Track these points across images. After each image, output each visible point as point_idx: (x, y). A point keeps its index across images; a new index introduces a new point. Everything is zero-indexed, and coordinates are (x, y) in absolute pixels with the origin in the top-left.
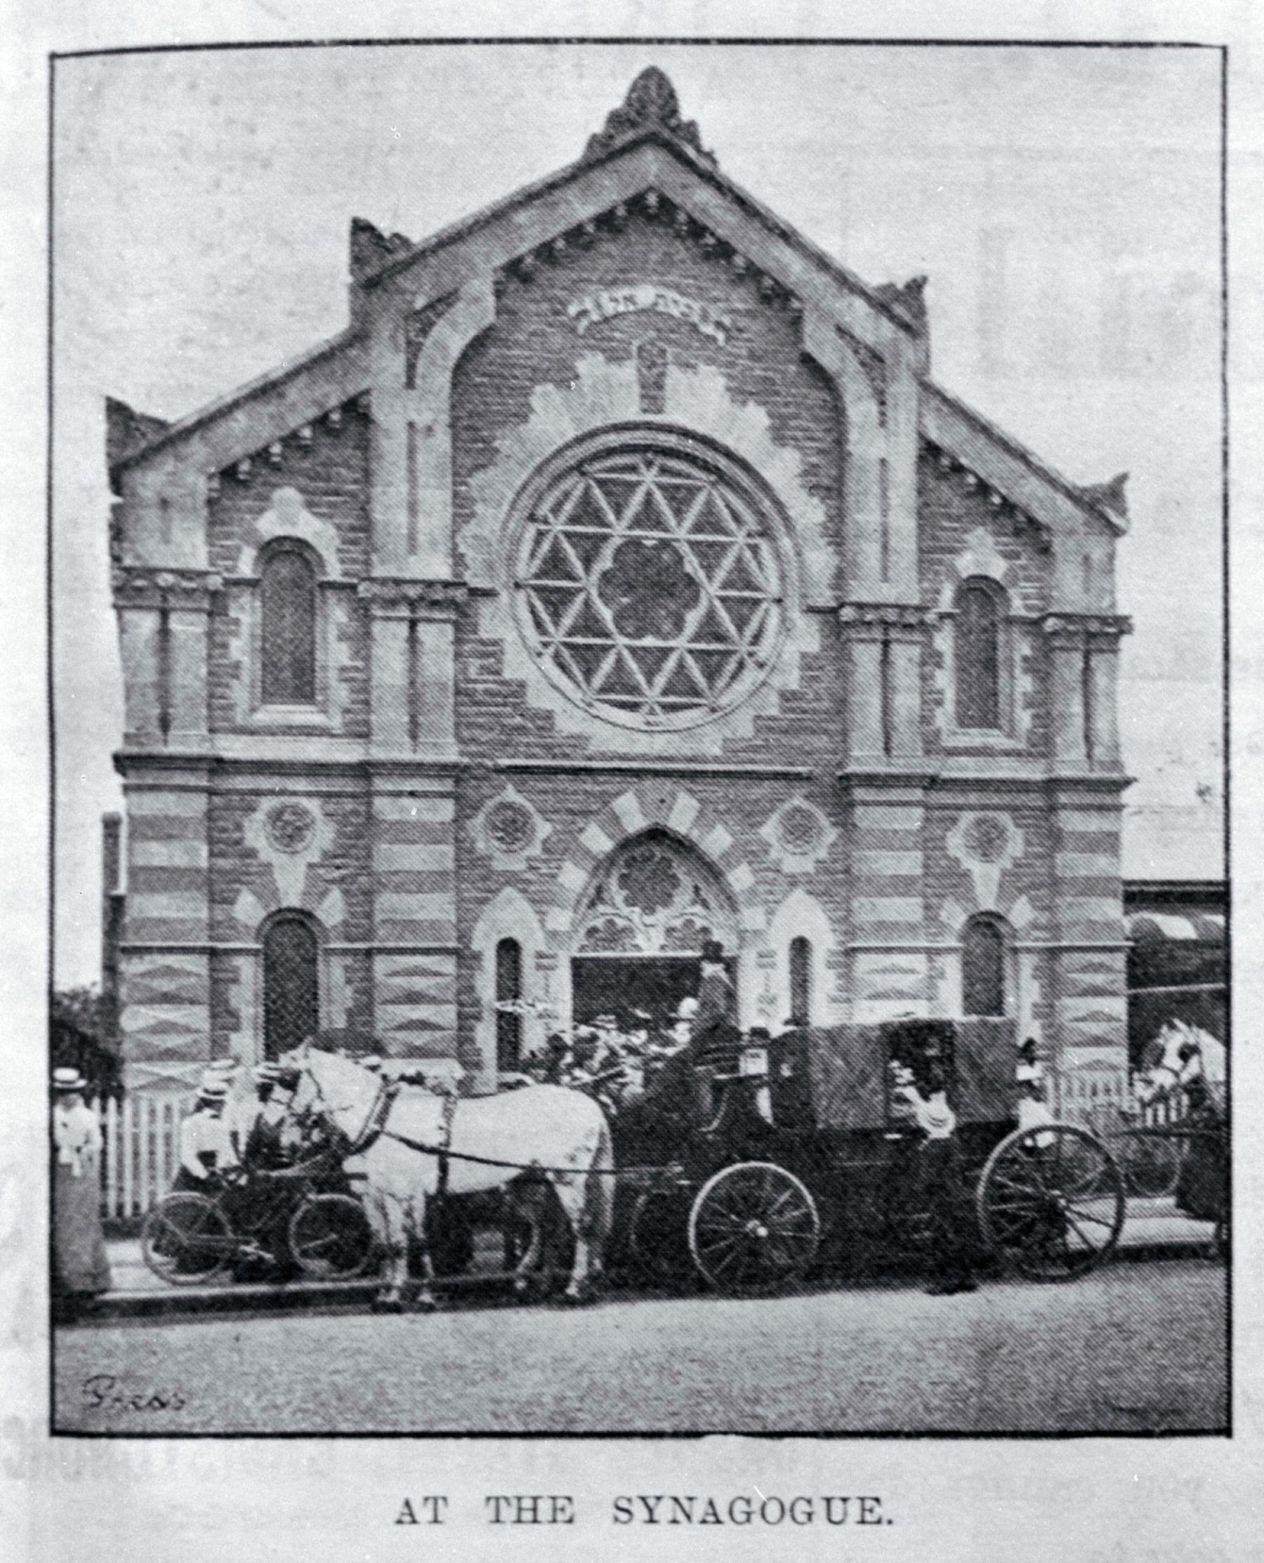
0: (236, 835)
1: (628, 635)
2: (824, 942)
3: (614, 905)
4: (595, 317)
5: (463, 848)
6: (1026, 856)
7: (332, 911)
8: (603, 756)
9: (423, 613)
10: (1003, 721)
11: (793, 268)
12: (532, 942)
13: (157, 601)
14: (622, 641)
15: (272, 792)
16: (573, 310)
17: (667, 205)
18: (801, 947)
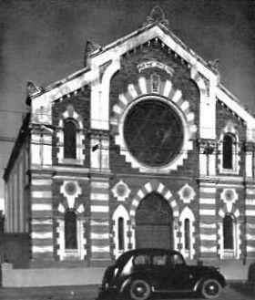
2: (192, 219)
5: (111, 195)
12: (126, 218)
17: (160, 41)
18: (187, 220)
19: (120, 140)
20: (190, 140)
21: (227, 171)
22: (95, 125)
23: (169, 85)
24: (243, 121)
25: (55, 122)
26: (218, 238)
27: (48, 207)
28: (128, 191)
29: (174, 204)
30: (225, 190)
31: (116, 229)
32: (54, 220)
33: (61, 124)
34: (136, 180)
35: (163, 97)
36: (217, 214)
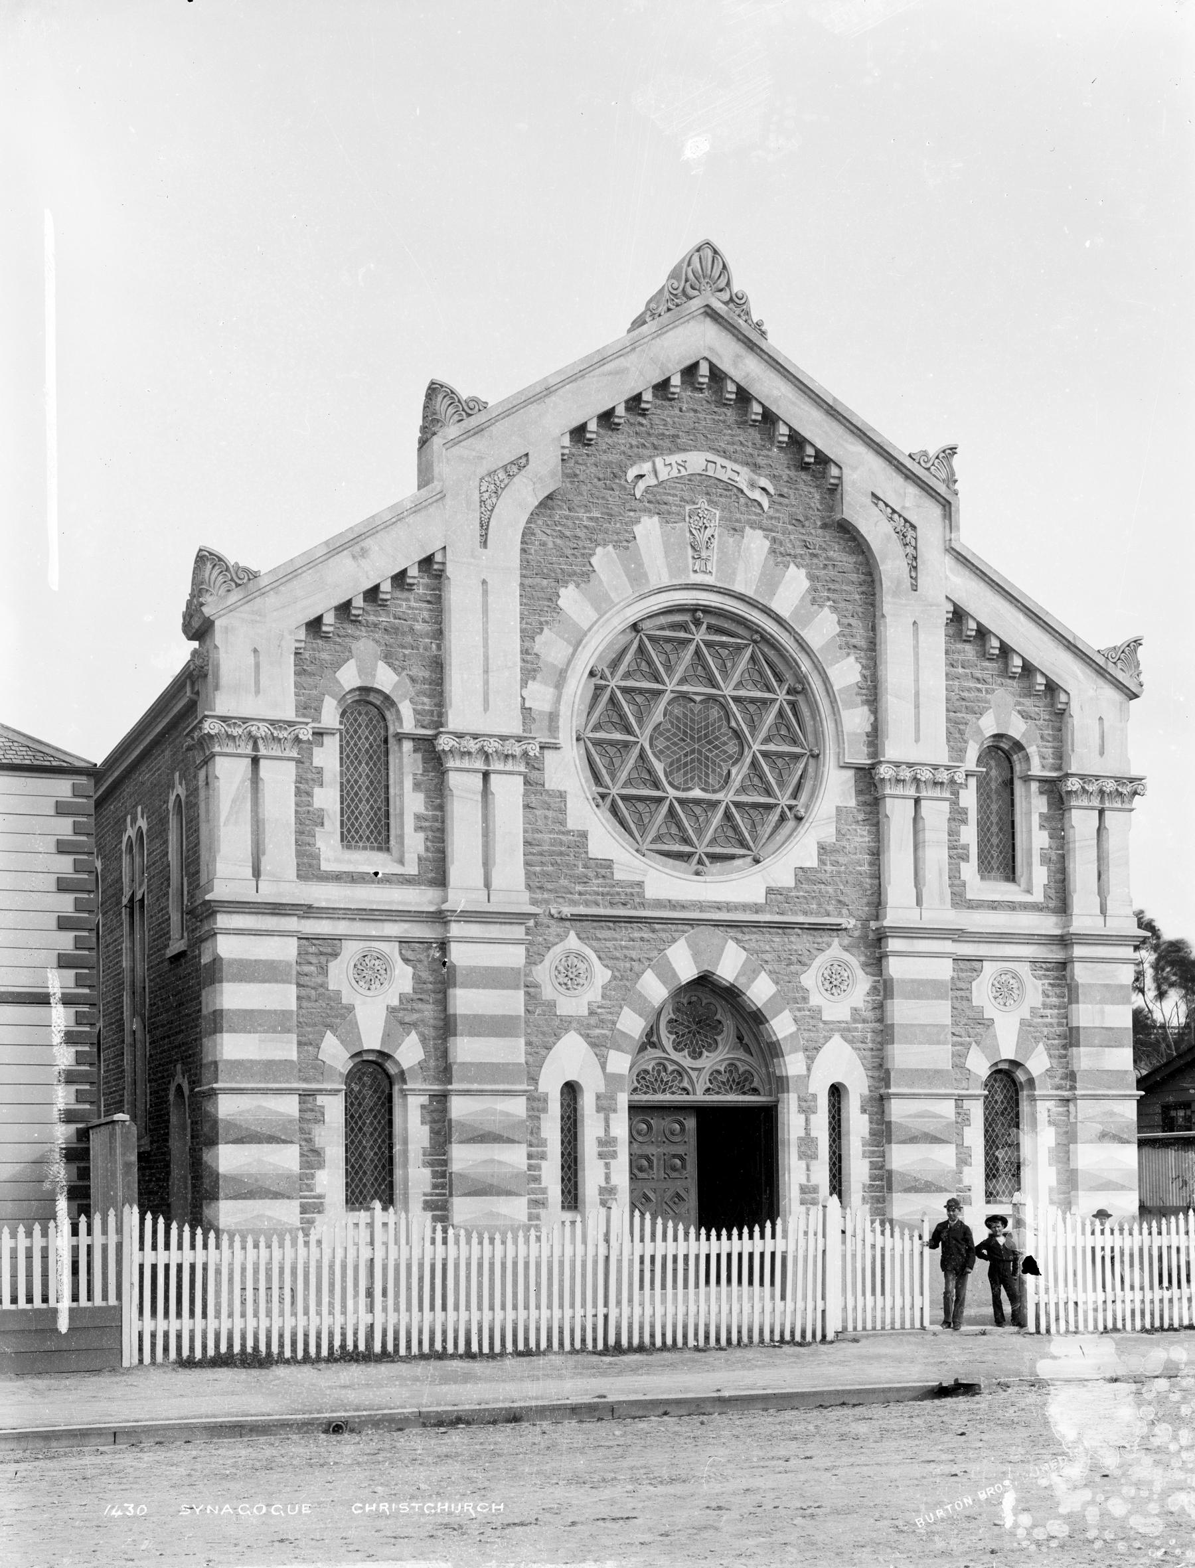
0: (319, 980)
2: (858, 1087)
3: (664, 1051)
4: (654, 482)
5: (532, 991)
7: (410, 1053)
8: (659, 904)
9: (497, 765)
10: (1023, 880)
11: (821, 434)
13: (249, 750)
14: (672, 793)
15: (994, 959)
16: (631, 473)
18: (836, 1092)
19: (566, 771)
23: (756, 544)
24: (1052, 688)
25: (309, 707)
26: (963, 1160)
27: (286, 1049)
28: (602, 975)
30: (351, 951)
32: (306, 1096)
33: (330, 716)
34: (626, 923)
35: (767, 611)
36: (959, 1064)
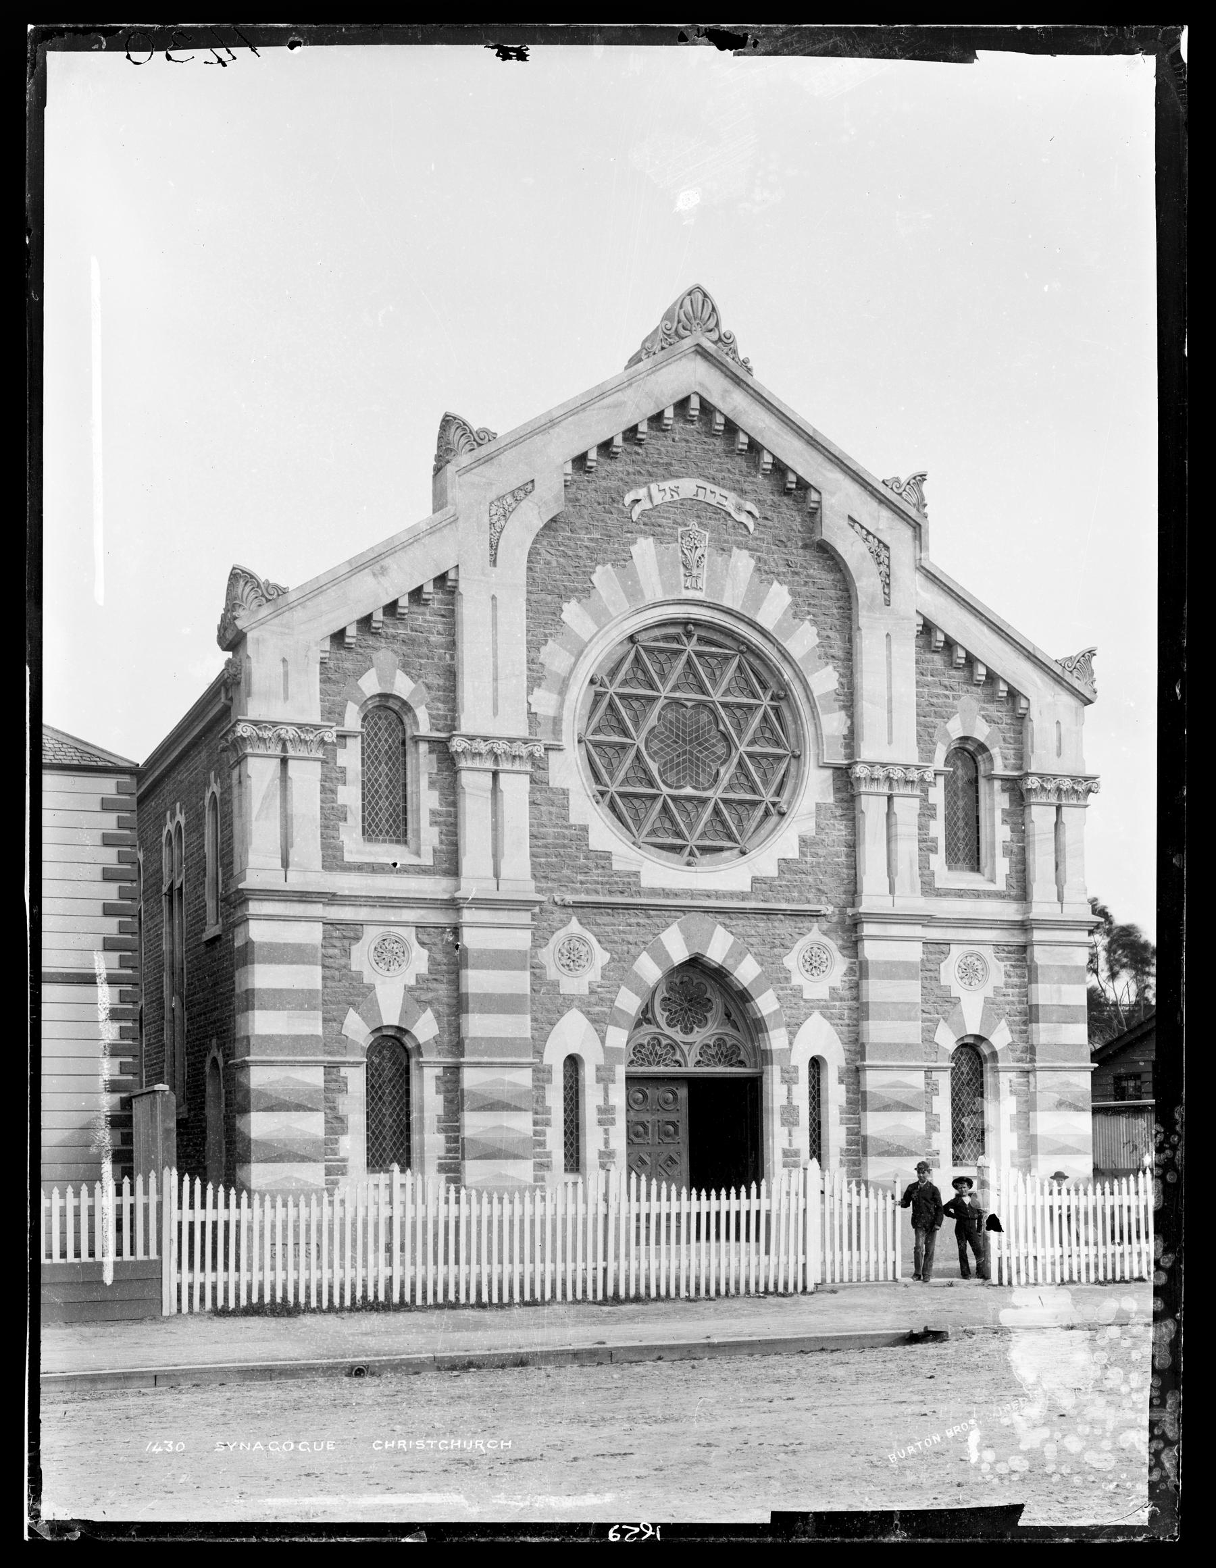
0: (343, 962)
1: (670, 786)
2: (836, 1060)
3: (659, 1027)
5: (537, 972)
6: (1007, 985)
8: (653, 892)
9: (505, 765)
10: (986, 870)
11: (802, 462)
13: (278, 751)
14: (666, 790)
16: (629, 498)
18: (816, 1064)
19: (569, 770)
20: (1081, 787)
21: (966, 880)
22: (475, 717)
23: (743, 562)
24: (1013, 695)
25: (333, 712)
26: (932, 1127)
27: (311, 1025)
28: (601, 957)
29: (766, 1004)
30: (371, 935)
31: (555, 1099)
32: (331, 1068)
34: (623, 910)
35: (753, 624)
36: (928, 1040)
